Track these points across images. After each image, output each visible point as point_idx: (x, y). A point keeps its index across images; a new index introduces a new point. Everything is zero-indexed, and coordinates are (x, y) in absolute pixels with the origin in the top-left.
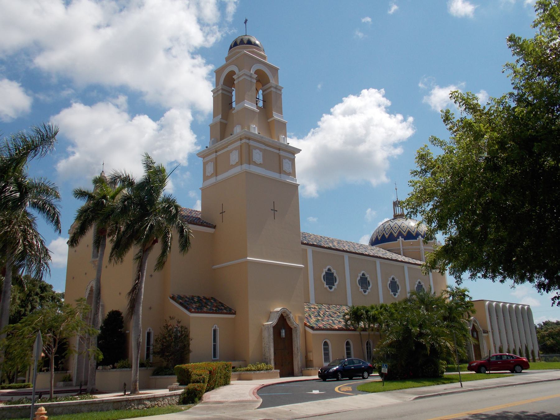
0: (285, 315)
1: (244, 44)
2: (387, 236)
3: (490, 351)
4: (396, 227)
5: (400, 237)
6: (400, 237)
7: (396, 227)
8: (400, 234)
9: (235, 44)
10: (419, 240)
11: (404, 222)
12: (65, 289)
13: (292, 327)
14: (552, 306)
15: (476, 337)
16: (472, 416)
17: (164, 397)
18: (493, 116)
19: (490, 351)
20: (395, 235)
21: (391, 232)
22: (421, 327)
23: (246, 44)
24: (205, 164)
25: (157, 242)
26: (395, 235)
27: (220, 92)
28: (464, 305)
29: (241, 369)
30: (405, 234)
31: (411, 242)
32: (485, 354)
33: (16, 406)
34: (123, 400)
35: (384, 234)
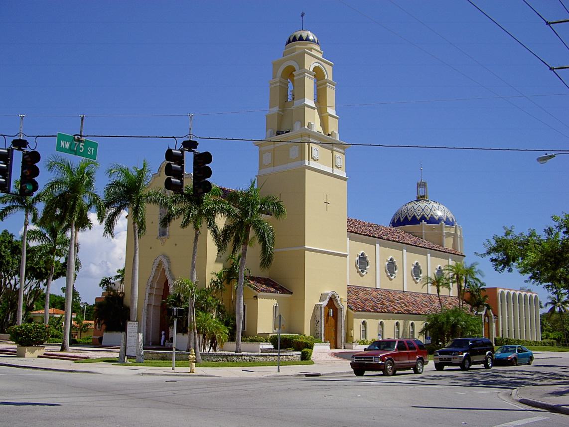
0: (333, 297)
1: (303, 40)
2: (402, 219)
3: (307, 376)
4: (419, 210)
5: (423, 221)
6: (423, 221)
7: (419, 210)
8: (423, 218)
9: (289, 42)
10: (422, 224)
11: (428, 205)
12: (21, 164)
13: (338, 308)
14: (163, 234)
15: (470, 367)
16: (101, 221)
17: (459, 392)
18: (28, 229)
19: (307, 376)
20: (419, 218)
21: (423, 215)
22: (163, 233)
23: (305, 40)
24: (261, 154)
25: (198, 144)
26: (419, 218)
27: (278, 84)
28: (360, 308)
29: (214, 332)
30: (428, 218)
31: (433, 226)
32: (146, 205)
33: (324, 334)
34: (490, 330)
35: (406, 216)
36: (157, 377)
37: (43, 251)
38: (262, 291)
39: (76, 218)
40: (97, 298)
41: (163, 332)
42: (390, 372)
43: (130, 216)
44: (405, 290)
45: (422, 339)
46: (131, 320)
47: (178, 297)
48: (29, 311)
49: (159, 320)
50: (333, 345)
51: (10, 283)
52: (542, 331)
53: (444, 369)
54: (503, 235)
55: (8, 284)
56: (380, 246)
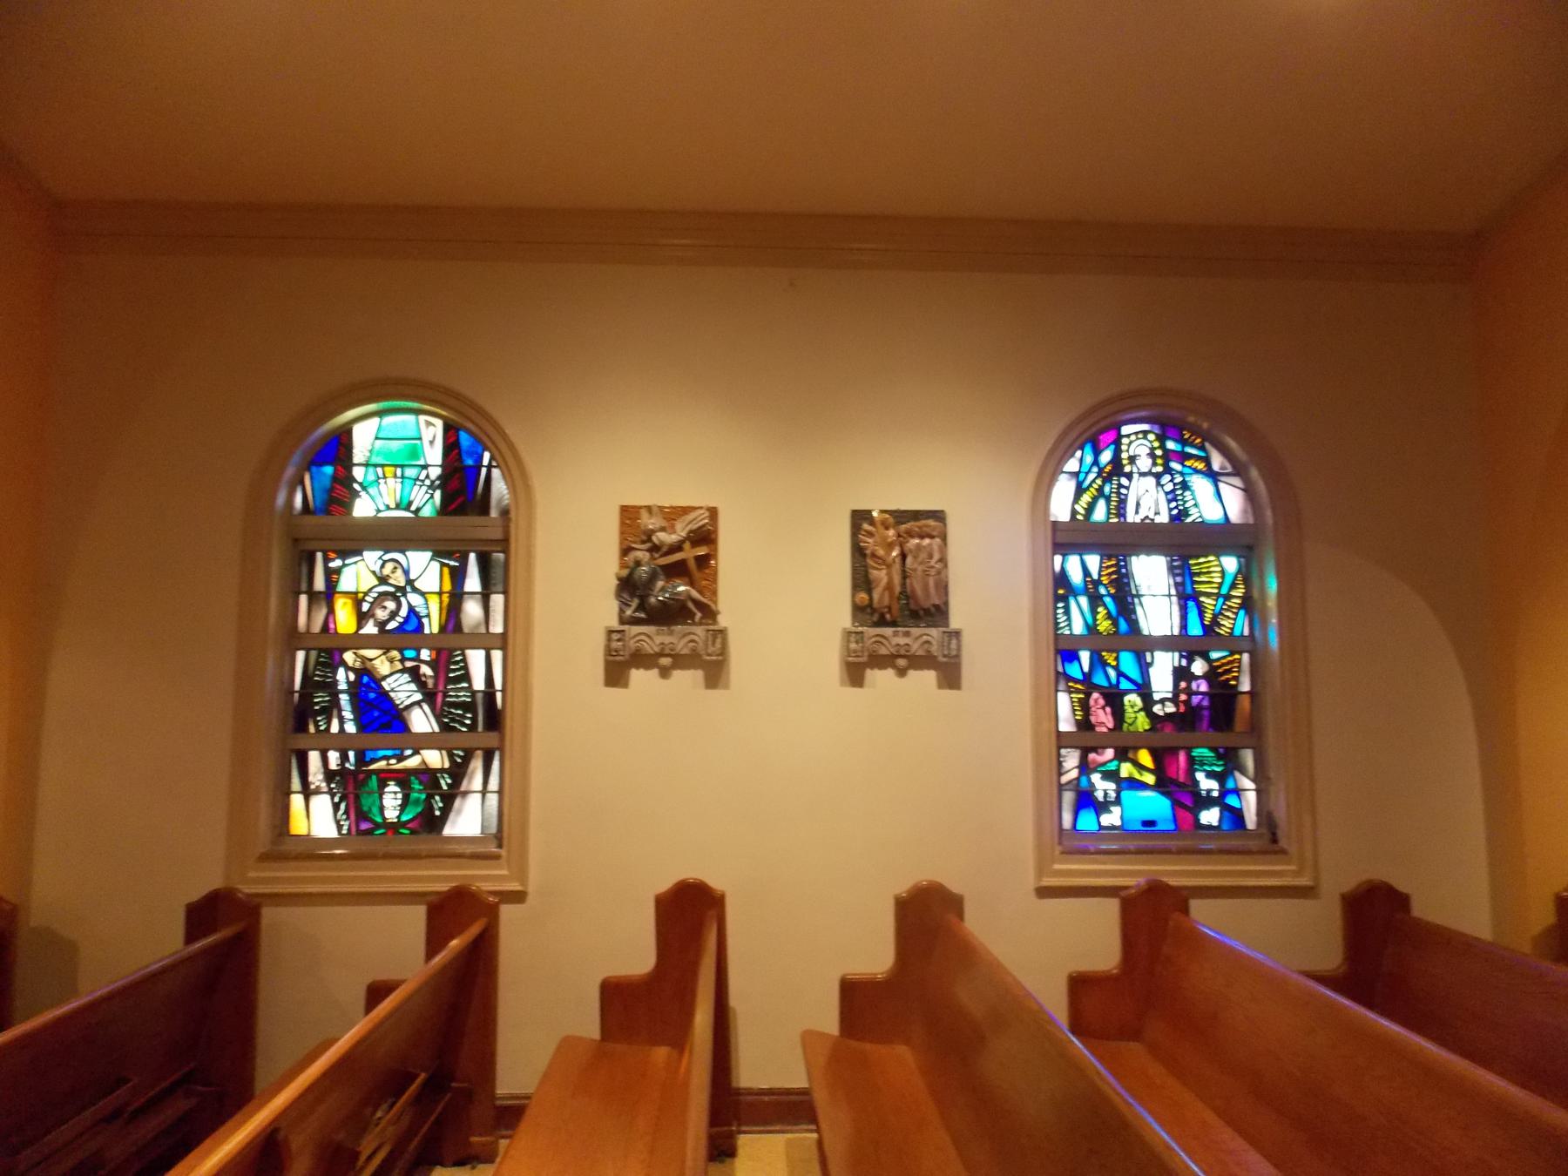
16: (1309, 975)
36: (1233, 483)
37: (945, 644)
38: (441, 602)
39: (681, 589)
40: (940, 686)
41: (1060, 605)
42: (1096, 701)
43: (1062, 552)
44: (438, 590)
45: (653, 600)
46: (1112, 906)
47: (1219, 622)
48: (297, 755)
49: (712, 1036)
50: (1061, 538)
51: (1120, 674)
52: (901, 517)
53: (367, 759)
54: (375, 513)
55: (1118, 682)
56: (400, 806)
